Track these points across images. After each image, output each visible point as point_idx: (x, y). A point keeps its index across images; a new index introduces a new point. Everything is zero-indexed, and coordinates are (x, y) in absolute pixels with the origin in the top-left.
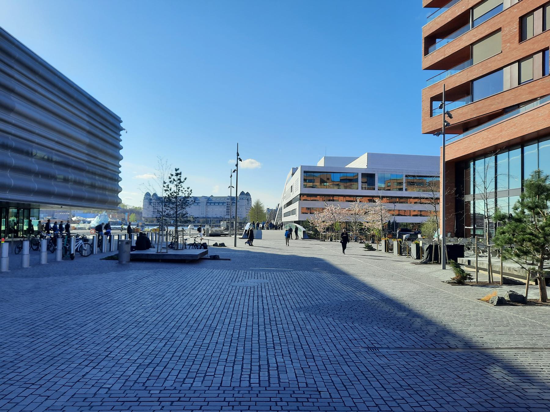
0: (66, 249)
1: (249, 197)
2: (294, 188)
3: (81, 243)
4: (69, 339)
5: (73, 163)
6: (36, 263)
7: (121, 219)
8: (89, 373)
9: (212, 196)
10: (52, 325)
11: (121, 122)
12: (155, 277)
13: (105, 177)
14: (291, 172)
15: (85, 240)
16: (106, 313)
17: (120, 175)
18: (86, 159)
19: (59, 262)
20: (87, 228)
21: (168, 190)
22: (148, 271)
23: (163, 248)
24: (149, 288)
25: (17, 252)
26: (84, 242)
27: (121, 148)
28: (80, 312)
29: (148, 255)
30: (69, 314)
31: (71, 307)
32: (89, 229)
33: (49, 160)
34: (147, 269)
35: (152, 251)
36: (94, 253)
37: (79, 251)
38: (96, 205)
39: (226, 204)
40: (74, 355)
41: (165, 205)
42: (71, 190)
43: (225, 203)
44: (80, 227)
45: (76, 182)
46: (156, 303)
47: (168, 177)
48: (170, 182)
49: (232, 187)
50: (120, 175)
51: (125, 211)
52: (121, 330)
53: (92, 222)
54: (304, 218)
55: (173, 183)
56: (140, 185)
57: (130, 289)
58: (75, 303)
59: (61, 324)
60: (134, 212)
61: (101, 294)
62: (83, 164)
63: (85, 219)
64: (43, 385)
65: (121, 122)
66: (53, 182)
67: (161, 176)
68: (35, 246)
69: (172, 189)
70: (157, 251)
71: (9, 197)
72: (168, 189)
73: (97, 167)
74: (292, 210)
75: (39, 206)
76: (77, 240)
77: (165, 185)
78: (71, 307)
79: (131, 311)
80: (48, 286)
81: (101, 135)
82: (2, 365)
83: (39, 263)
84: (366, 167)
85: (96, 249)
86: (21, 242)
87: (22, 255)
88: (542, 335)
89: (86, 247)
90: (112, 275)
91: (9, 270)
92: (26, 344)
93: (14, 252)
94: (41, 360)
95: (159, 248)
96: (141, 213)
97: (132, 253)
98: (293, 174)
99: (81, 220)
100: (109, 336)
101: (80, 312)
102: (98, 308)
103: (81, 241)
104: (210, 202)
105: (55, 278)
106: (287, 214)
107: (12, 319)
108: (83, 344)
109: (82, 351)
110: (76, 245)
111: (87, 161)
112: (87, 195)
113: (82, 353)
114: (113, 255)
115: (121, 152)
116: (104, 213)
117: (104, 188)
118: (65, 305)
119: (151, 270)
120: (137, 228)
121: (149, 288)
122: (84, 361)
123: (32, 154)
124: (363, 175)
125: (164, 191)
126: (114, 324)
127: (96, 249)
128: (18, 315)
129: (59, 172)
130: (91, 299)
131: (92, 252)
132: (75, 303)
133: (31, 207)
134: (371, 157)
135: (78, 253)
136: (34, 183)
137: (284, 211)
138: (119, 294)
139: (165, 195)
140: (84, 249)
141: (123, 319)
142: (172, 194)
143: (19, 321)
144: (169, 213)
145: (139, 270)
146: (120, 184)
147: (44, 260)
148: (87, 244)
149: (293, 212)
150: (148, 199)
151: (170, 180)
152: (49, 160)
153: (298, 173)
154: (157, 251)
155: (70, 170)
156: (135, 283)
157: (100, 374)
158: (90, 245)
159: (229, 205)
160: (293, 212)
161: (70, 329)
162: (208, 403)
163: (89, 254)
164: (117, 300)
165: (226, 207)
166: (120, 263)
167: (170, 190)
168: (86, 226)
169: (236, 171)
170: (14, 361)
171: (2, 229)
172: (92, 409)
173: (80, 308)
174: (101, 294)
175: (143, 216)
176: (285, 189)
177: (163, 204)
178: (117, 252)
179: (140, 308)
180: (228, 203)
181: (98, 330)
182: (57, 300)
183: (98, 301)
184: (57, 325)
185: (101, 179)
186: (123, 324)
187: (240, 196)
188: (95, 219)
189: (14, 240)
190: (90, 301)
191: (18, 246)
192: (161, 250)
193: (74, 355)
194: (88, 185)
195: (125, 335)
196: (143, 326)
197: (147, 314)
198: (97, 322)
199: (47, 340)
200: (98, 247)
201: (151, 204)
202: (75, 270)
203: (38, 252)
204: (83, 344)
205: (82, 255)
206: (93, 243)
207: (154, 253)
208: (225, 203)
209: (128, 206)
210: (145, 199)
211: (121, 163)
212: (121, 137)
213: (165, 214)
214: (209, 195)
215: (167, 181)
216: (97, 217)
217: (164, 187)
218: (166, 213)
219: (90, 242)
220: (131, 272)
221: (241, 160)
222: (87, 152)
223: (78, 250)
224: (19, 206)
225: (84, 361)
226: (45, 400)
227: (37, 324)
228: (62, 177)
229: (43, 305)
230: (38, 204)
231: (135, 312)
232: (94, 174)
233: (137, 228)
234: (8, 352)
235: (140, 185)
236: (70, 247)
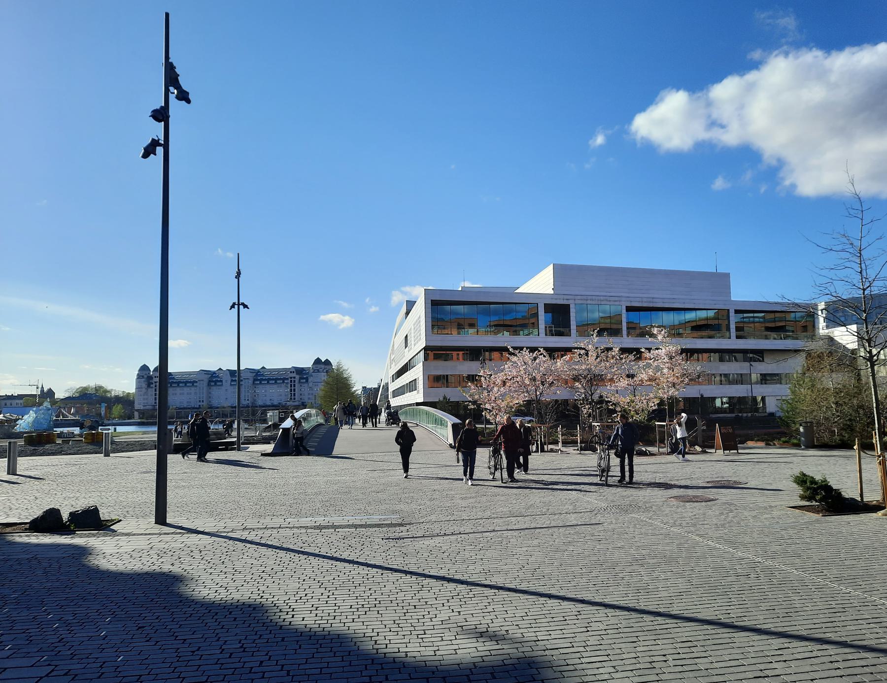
1: (329, 367)
2: (411, 340)
9: (263, 368)
14: (404, 310)
39: (289, 381)
43: (288, 379)
49: (241, 307)
54: (439, 394)
74: (408, 382)
84: (552, 292)
88: (767, 553)
98: (407, 313)
104: (259, 378)
106: (398, 392)
124: (549, 308)
134: (562, 273)
137: (392, 387)
149: (411, 386)
150: (146, 376)
153: (420, 310)
159: (294, 381)
160: (411, 386)
162: (292, 680)
165: (289, 385)
169: (160, 150)
172: (181, 627)
176: (393, 345)
180: (293, 379)
187: (314, 366)
201: (152, 386)
208: (288, 379)
210: (139, 377)
214: (258, 367)
221: (184, 96)
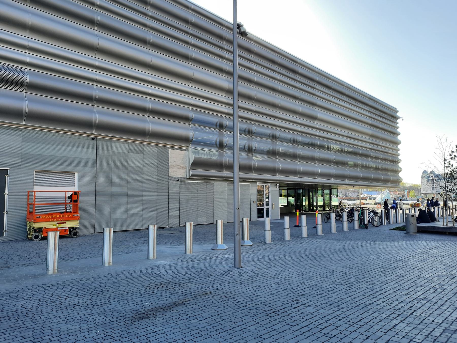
0: (361, 220)
3: (372, 215)
4: (376, 293)
5: (360, 152)
6: (340, 230)
7: (401, 196)
8: (398, 325)
10: (361, 279)
11: (397, 112)
12: (445, 248)
13: (386, 160)
15: (375, 213)
16: (404, 276)
17: (399, 157)
18: (370, 147)
19: (357, 230)
20: (373, 203)
21: (449, 167)
22: (435, 242)
23: (448, 222)
24: (440, 258)
25: (326, 221)
26: (375, 214)
27: (398, 134)
28: (381, 272)
29: (434, 227)
30: (372, 273)
31: (372, 267)
32: (375, 204)
33: (343, 151)
34: (434, 240)
35: (438, 224)
36: (384, 224)
37: (371, 221)
38: (380, 184)
40: (383, 307)
41: (447, 181)
42: (359, 173)
44: (367, 203)
45: (363, 166)
46: (451, 273)
47: (449, 154)
48: (451, 158)
50: (399, 157)
51: (404, 189)
52: (420, 293)
53: (377, 198)
55: (454, 159)
56: (421, 164)
57: (421, 257)
58: (375, 264)
59: (367, 279)
60: (413, 189)
61: (396, 259)
62: (368, 151)
63: (371, 196)
64: (362, 326)
65: (397, 112)
66: (346, 168)
67: (441, 154)
68: (339, 217)
69: (453, 165)
70: (443, 224)
71: (318, 181)
72: (450, 166)
73: (379, 152)
75: (337, 186)
76: (369, 213)
77: (446, 162)
78: (372, 267)
79: (426, 277)
80: (351, 248)
81: (381, 125)
82: (331, 304)
83: (342, 230)
85: (385, 221)
86: (329, 214)
87: (331, 223)
89: (377, 219)
90: (402, 244)
91: (323, 234)
92: (344, 290)
93: (324, 221)
94: (357, 306)
95: (445, 222)
96: (420, 190)
97: (418, 225)
99: (367, 197)
100: (410, 297)
101: (381, 272)
102: (395, 271)
103: (372, 214)
105: (356, 242)
107: (331, 270)
108: (388, 300)
109: (388, 305)
110: (368, 217)
111: (371, 149)
112: (372, 176)
113: (389, 307)
114: (400, 226)
115: (399, 137)
116: (387, 190)
117: (386, 170)
118: (367, 265)
119: (439, 242)
120: (418, 203)
121: (440, 258)
122: (392, 314)
123: (330, 148)
125: (446, 168)
126: (412, 286)
127: (385, 221)
128: (334, 268)
129: (351, 160)
130: (387, 262)
131: (381, 223)
132: (375, 264)
133: (332, 187)
135: (371, 224)
136: (332, 170)
138: (412, 261)
139: (447, 171)
140: (375, 221)
141: (420, 284)
142: (454, 170)
143: (336, 273)
144: (453, 189)
145: (427, 240)
146: (400, 165)
147: (346, 229)
148: (377, 216)
151: (451, 157)
152: (343, 151)
154: (443, 224)
155: (358, 157)
156: (426, 253)
157: (409, 329)
158: (380, 218)
161: (375, 285)
163: (379, 225)
164: (411, 266)
166: (407, 233)
167: (452, 166)
168: (373, 201)
170: (338, 302)
171: (314, 204)
173: (380, 269)
174: (396, 259)
175: (422, 192)
177: (446, 180)
178: (404, 224)
179: (435, 275)
181: (399, 290)
182: (361, 260)
183: (394, 265)
184: (364, 279)
185: (384, 162)
186: (421, 288)
188: (379, 196)
189: (324, 212)
190: (387, 264)
191: (326, 216)
192: (447, 223)
193: (383, 307)
194: (373, 168)
195: (425, 298)
196: (441, 293)
197: (444, 283)
198: (396, 283)
199: (359, 291)
200: (386, 219)
202: (370, 237)
203: (340, 222)
204: (388, 300)
205: (374, 225)
206: (382, 215)
207: (441, 226)
209: (407, 184)
211: (399, 147)
212: (398, 125)
213: (448, 190)
215: (448, 158)
216: (381, 194)
217: (445, 163)
218: (449, 188)
219: (379, 215)
220: (419, 242)
222: (370, 141)
223: (371, 221)
224: (324, 187)
225: (392, 314)
226: (366, 339)
227: (349, 277)
228: (353, 163)
229: (351, 263)
230: (337, 185)
231: (430, 278)
232: (377, 158)
233: (418, 203)
234: (333, 295)
235: (421, 164)
236: (364, 218)
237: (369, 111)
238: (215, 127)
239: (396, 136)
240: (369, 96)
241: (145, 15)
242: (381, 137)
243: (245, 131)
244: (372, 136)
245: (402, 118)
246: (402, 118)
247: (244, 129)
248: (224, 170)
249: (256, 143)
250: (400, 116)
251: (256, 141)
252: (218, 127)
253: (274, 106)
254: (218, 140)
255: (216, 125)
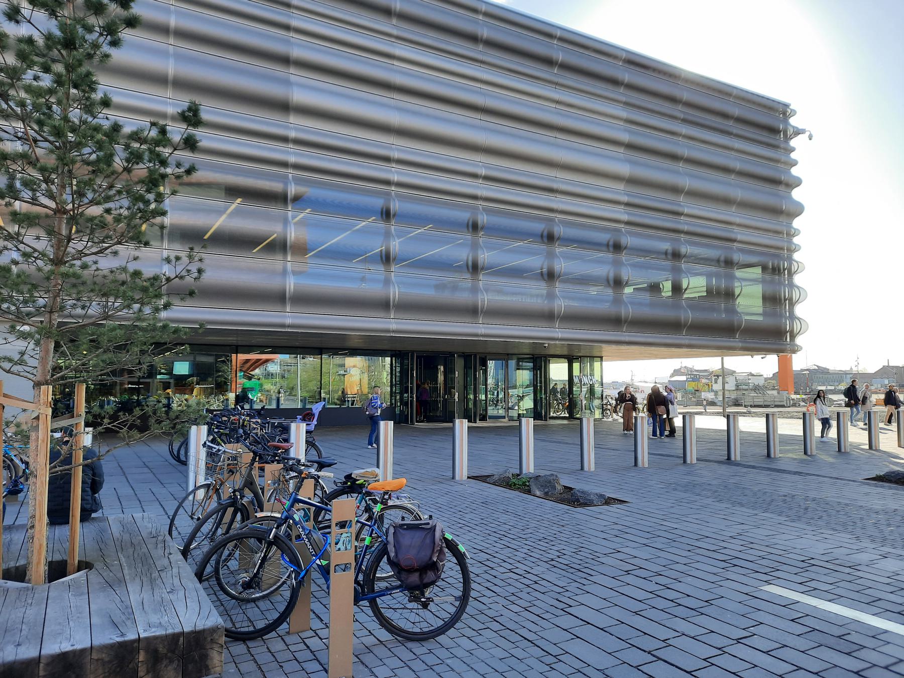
111: (628, 223)
211: (797, 223)
212: (793, 155)
237: (626, 104)
238: (664, 256)
239: (782, 188)
240: (624, 55)
241: (728, 133)
242: (739, 200)
243: (542, 236)
244: (632, 181)
245: (807, 134)
246: (807, 134)
247: (606, 242)
248: (481, 319)
249: (630, 271)
250: (800, 127)
251: (631, 265)
252: (611, 249)
253: (727, 201)
254: (470, 259)
255: (542, 236)
